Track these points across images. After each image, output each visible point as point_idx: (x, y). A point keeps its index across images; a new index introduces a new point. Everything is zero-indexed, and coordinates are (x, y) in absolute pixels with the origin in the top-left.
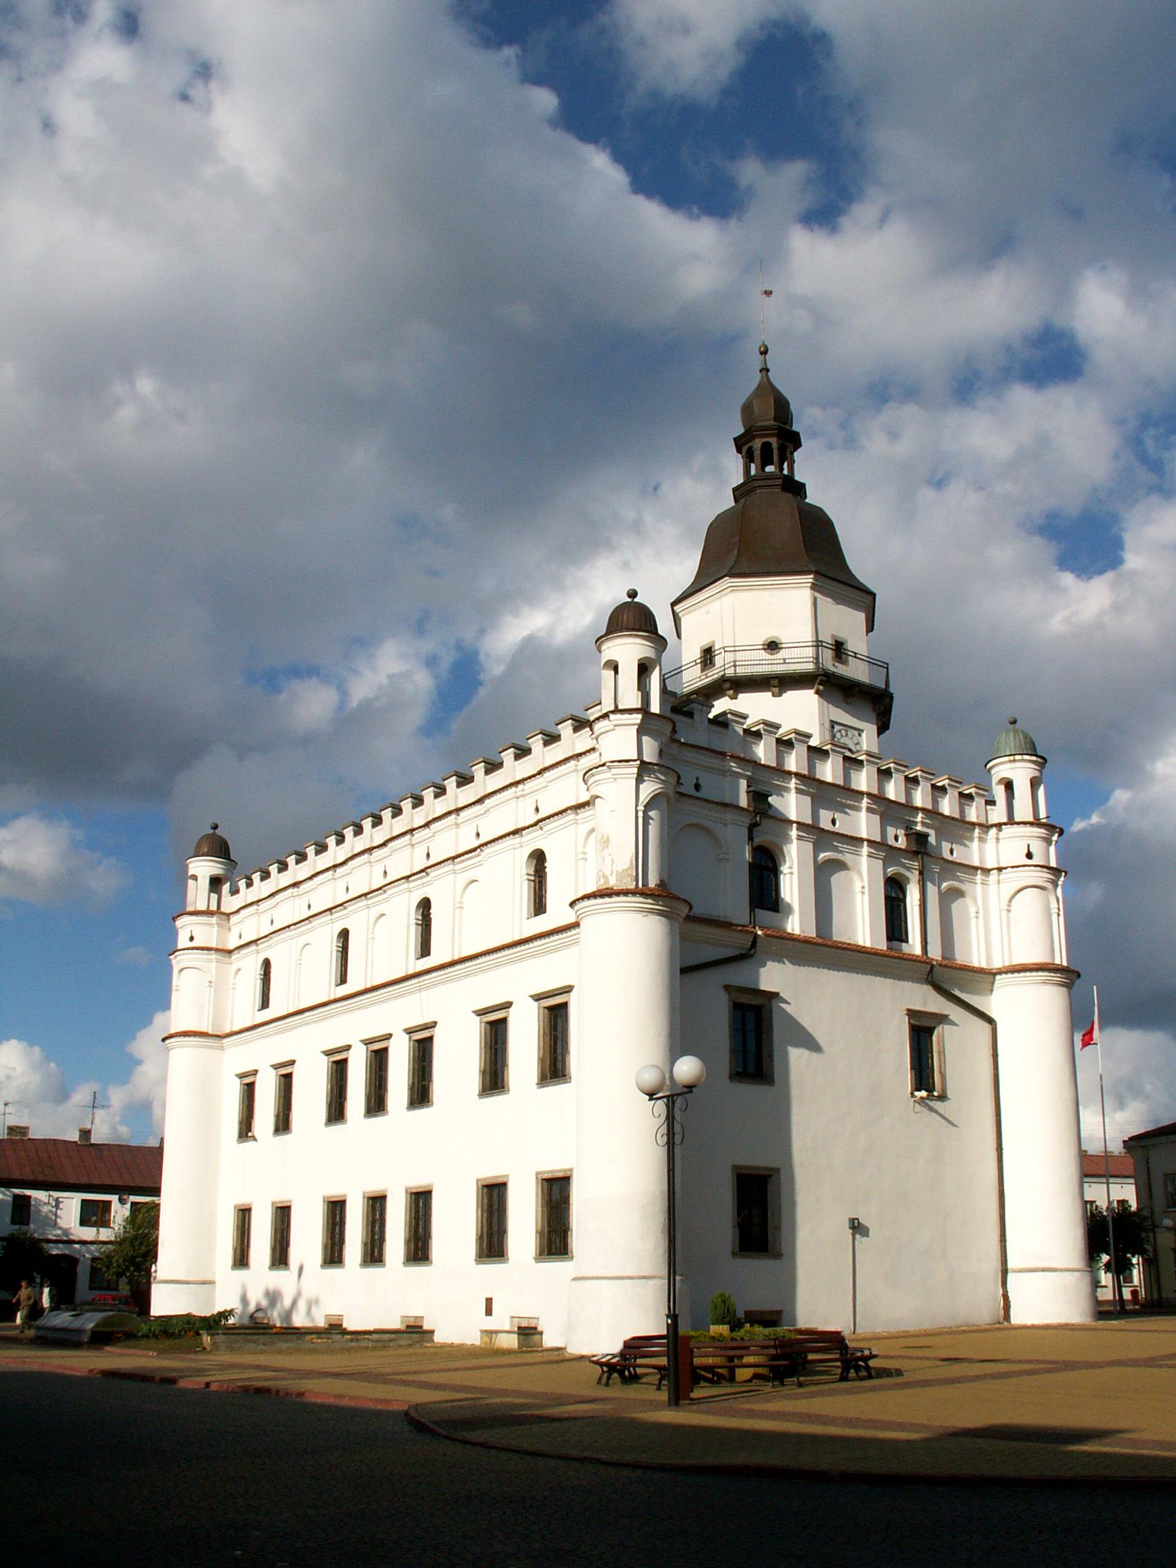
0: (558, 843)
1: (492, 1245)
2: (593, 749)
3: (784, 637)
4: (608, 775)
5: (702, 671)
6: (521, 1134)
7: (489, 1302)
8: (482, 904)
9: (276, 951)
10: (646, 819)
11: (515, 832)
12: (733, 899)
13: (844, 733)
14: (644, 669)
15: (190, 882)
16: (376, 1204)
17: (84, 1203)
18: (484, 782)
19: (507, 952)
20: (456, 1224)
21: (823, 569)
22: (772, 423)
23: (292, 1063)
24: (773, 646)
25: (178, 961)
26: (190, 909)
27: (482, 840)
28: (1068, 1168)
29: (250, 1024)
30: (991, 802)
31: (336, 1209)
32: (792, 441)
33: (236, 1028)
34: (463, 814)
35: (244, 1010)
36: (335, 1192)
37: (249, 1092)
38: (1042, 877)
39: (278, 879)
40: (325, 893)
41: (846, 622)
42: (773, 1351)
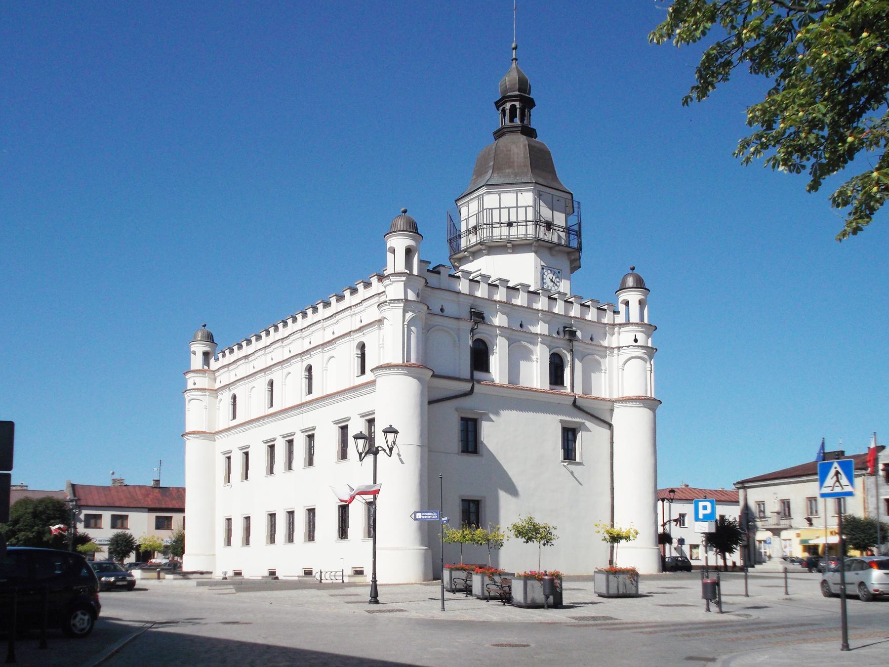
0: (370, 339)
8: (337, 370)
9: (238, 390)
10: (409, 331)
14: (409, 252)
15: (390, 256)
17: (113, 516)
21: (540, 181)
22: (517, 93)
26: (192, 368)
28: (649, 498)
30: (616, 312)
32: (528, 103)
35: (223, 420)
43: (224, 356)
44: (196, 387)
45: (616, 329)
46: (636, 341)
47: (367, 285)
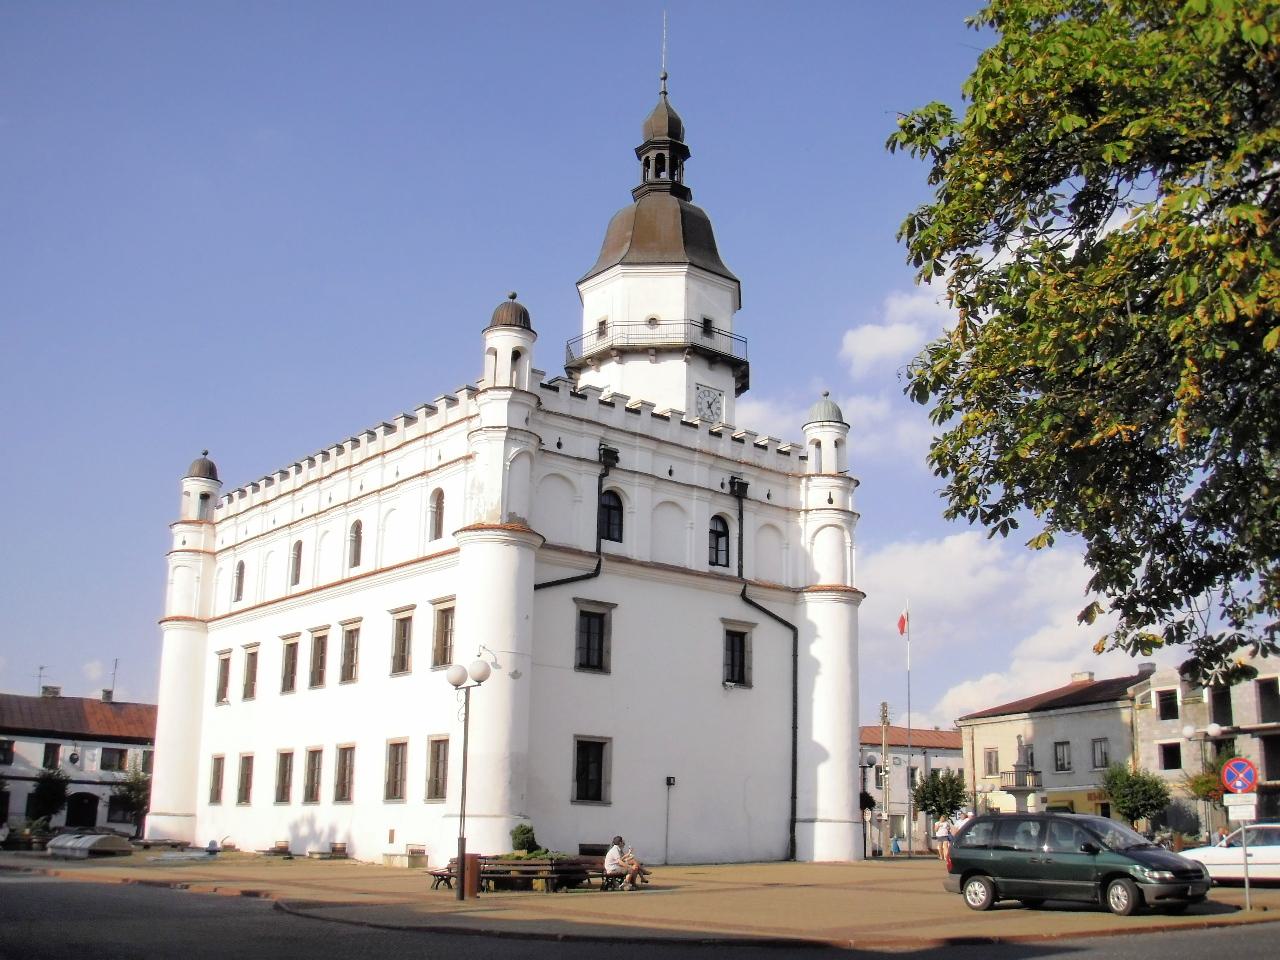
0: (452, 484)
1: (394, 789)
2: (478, 415)
3: (662, 316)
4: (485, 437)
5: (598, 339)
6: (421, 707)
7: (392, 833)
8: (398, 529)
11: (423, 474)
12: (583, 530)
13: (707, 393)
14: (516, 355)
15: (490, 358)
16: (315, 756)
18: (405, 432)
19: (413, 566)
20: (370, 773)
21: (697, 261)
23: (360, 620)
24: (653, 322)
25: (174, 560)
27: (400, 478)
29: (227, 612)
31: (286, 759)
32: (680, 153)
33: (218, 615)
34: (389, 456)
35: (222, 600)
36: (286, 747)
37: (225, 665)
38: (836, 518)
39: (280, 486)
40: (284, 512)
41: (716, 302)
42: (550, 868)
43: (231, 500)
44: (186, 547)
45: (804, 480)
46: (830, 501)
47: (452, 401)
